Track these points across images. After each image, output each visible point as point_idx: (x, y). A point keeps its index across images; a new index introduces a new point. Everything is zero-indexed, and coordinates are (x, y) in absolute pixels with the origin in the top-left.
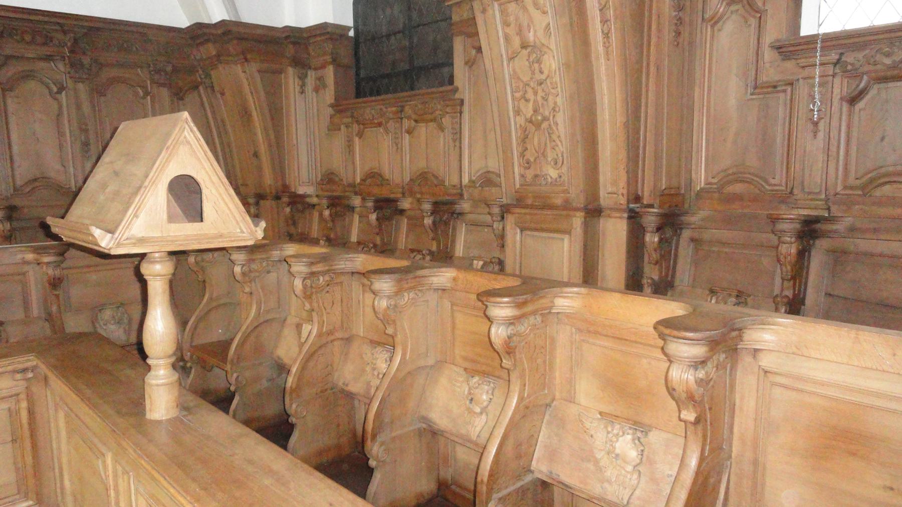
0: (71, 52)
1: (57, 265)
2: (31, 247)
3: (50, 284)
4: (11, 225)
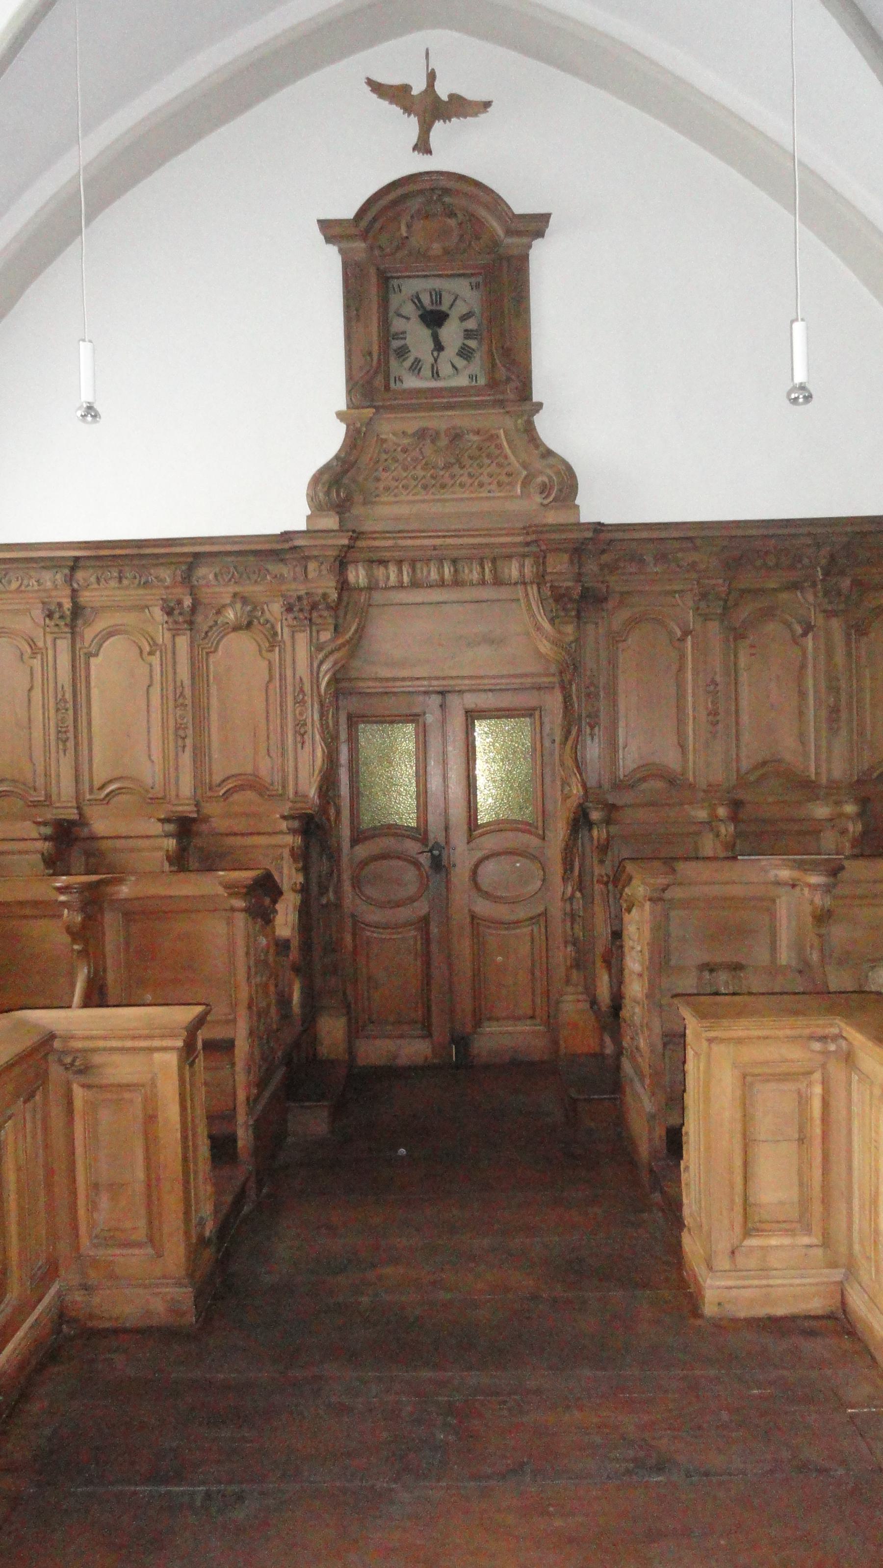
0: (827, 574)
1: (828, 889)
2: (795, 861)
3: (814, 917)
4: (735, 828)
